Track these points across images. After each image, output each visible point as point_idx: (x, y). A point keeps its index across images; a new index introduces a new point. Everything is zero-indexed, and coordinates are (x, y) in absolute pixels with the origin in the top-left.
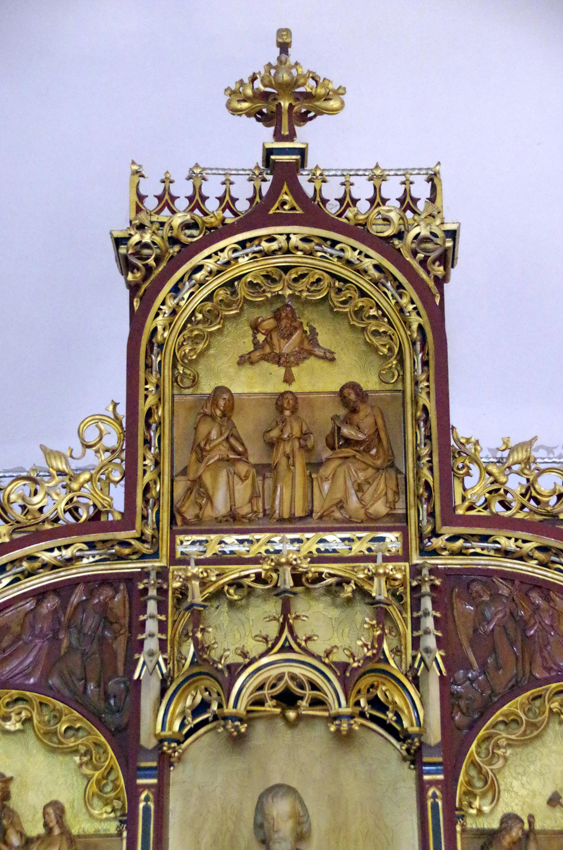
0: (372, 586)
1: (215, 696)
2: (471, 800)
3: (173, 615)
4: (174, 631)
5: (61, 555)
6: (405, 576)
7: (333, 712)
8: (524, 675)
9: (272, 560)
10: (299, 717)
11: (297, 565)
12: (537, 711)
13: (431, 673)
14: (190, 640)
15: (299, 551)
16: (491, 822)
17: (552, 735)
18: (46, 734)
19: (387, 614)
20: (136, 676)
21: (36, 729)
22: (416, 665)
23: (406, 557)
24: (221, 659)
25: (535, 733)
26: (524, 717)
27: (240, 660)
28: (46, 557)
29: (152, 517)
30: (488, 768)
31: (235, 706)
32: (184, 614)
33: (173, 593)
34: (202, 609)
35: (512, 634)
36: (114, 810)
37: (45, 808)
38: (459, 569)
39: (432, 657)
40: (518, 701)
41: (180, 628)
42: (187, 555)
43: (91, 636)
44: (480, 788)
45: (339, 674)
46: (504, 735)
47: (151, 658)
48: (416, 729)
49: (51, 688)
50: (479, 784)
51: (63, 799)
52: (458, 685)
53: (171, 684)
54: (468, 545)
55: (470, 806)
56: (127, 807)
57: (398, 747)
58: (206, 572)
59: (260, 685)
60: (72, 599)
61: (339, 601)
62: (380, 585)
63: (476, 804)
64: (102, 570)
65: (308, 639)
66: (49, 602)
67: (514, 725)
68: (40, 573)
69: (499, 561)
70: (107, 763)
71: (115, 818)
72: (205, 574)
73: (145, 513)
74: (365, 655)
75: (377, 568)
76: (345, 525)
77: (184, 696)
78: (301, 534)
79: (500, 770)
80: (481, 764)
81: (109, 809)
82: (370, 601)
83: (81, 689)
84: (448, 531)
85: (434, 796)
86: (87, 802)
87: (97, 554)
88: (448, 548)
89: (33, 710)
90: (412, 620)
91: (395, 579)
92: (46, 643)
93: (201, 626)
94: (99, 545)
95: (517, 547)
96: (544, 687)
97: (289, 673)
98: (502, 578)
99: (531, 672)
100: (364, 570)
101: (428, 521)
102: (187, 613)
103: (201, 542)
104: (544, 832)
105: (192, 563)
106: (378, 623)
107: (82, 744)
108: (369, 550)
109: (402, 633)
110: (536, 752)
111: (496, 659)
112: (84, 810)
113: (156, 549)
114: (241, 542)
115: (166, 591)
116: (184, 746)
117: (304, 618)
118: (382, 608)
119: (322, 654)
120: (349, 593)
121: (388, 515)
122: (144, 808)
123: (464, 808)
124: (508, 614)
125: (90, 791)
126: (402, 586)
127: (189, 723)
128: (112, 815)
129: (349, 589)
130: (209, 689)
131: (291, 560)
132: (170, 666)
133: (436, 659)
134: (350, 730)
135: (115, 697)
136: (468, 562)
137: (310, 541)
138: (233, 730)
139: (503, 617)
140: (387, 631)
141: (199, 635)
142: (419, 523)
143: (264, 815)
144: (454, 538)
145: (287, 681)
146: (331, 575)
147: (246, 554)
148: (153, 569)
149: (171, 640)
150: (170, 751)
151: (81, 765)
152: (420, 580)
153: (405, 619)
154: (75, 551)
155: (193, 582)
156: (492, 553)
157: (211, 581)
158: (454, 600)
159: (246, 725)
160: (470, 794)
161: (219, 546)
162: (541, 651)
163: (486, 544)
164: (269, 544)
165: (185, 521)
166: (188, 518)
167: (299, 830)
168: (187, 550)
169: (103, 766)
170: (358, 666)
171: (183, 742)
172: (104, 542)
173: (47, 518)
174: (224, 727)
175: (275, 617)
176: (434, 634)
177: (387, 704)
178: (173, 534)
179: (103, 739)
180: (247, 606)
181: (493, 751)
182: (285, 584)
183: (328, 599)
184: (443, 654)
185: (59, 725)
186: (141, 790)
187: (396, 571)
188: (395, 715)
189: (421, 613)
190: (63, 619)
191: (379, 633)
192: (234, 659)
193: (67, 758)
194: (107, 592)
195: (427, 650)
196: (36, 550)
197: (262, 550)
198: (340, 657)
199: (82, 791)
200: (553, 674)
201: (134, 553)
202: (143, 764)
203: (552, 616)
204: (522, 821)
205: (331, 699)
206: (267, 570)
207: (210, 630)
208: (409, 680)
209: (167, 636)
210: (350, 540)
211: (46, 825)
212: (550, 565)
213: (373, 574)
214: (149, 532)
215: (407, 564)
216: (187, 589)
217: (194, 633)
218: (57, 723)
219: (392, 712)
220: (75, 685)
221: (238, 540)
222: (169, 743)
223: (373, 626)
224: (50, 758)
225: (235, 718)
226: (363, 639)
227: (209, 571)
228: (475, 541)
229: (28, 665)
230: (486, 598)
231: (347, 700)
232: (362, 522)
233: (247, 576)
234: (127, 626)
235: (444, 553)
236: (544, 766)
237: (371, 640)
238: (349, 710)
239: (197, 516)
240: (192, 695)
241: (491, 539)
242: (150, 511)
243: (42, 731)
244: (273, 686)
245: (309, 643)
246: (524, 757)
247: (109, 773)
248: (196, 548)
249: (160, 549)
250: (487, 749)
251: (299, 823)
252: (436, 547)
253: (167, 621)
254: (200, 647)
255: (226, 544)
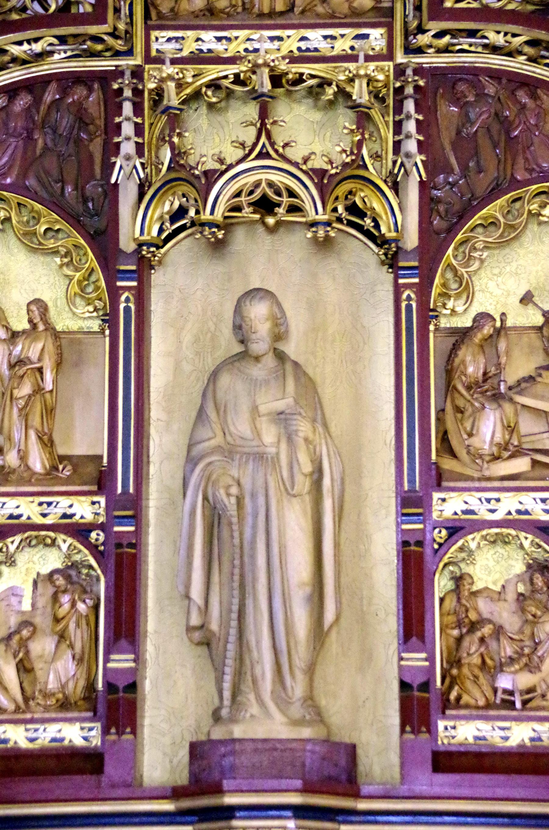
0: (353, 87)
1: (192, 202)
2: (446, 302)
3: (150, 118)
4: (151, 136)
5: (30, 49)
6: (388, 76)
7: (310, 219)
8: (505, 179)
9: (249, 62)
10: (279, 224)
11: (275, 66)
12: (516, 213)
13: (411, 178)
14: (167, 144)
15: (279, 50)
16: (465, 321)
17: (530, 236)
18: (25, 234)
19: (368, 117)
20: (113, 181)
21: (16, 230)
22: (396, 171)
23: (390, 56)
24: (198, 164)
25: (513, 235)
26: (502, 220)
27: (217, 166)
28: (15, 50)
29: (125, 10)
30: (463, 270)
31: (212, 213)
32: (161, 117)
33: (150, 94)
34: (178, 112)
35: (496, 137)
36: (96, 310)
37: (29, 304)
38: (446, 67)
39: (412, 162)
40: (497, 204)
41: (157, 132)
42: (163, 53)
43: (66, 136)
44: (456, 290)
45: (316, 181)
46: (482, 238)
47: (128, 162)
48: (393, 234)
49: (27, 188)
50: (454, 286)
51: (45, 298)
52: (439, 190)
53: (148, 190)
54: (455, 41)
55: (444, 306)
56: (108, 307)
57: (377, 251)
58: (182, 73)
59: (238, 192)
60: (44, 98)
61: (320, 103)
62: (361, 86)
63: (450, 305)
64: (76, 67)
65: (286, 145)
66: (22, 99)
67: (492, 228)
68: (11, 68)
69: (488, 58)
70: (87, 265)
71: (98, 317)
72: (181, 75)
73: (117, 5)
74: (344, 161)
75: (358, 68)
76: (327, 21)
77: (162, 202)
78: (281, 31)
79: (475, 272)
80: (457, 267)
81: (91, 308)
82: (350, 104)
83: (59, 191)
84: (435, 26)
85: (409, 298)
86: (70, 301)
87: (69, 50)
88: (434, 45)
89: (11, 209)
90: (394, 124)
91: (377, 81)
92: (20, 143)
93: (178, 131)
94: (70, 40)
95: (506, 42)
96: (524, 189)
97: (266, 179)
98: (489, 77)
99: (512, 175)
100: (345, 71)
101: (414, 16)
102: (163, 116)
103: (177, 39)
104: (515, 328)
105: (168, 62)
106: (358, 128)
107: (62, 246)
108: (352, 48)
109: (383, 138)
110: (513, 253)
111: (478, 163)
112: (67, 309)
113: (130, 45)
114: (219, 39)
115: (142, 92)
116: (163, 251)
117: (282, 124)
118: (362, 112)
119: (300, 161)
120: (330, 95)
121: (373, 8)
122: (125, 308)
123: (438, 310)
124: (493, 114)
125: (71, 292)
126: (385, 87)
127: (168, 229)
128: (95, 314)
129: (330, 91)
130: (187, 196)
131: (269, 61)
132: (148, 170)
133: (416, 164)
134: (327, 238)
135: (93, 200)
136: (455, 60)
137: (291, 39)
138: (210, 236)
139: (487, 119)
140: (367, 136)
141: (176, 140)
142: (404, 19)
143: (242, 318)
144: (439, 35)
145: (264, 188)
146: (313, 77)
147: (224, 53)
148: (127, 68)
149: (148, 143)
150: (149, 255)
151: (61, 266)
152: (403, 81)
153: (387, 123)
154: (45, 45)
155: (169, 83)
156: (480, 49)
157: (187, 83)
158: (438, 102)
159: (223, 232)
160: (445, 295)
161: (196, 43)
162: (524, 152)
163: (473, 40)
164: (248, 42)
165: (160, 16)
166: (164, 12)
167: (277, 331)
168: (162, 47)
169: (83, 268)
170: (336, 173)
171: (162, 247)
172: (75, 36)
173: (14, 7)
174: (201, 233)
175: (252, 122)
176: (415, 138)
177: (365, 211)
178: (148, 29)
179: (82, 242)
180: (226, 109)
181: (469, 253)
182: (263, 87)
183: (310, 101)
184: (424, 158)
185: (38, 227)
186: (121, 292)
187: (378, 72)
188: (373, 221)
189: (402, 137)
190: (36, 118)
191: (359, 137)
192: (212, 165)
193: (48, 259)
194: (80, 92)
195: (408, 155)
196: (4, 43)
197: (241, 49)
198: (318, 163)
199: (64, 290)
200: (534, 175)
201: (107, 50)
202: (122, 268)
203: (538, 115)
204: (494, 320)
205: (308, 206)
206: (245, 72)
207: (187, 134)
208: (388, 186)
209: (144, 139)
210: (333, 38)
211: (30, 321)
212: (539, 60)
213: (354, 75)
214: (122, 26)
215: (391, 64)
216: (163, 90)
217: (171, 137)
218: (37, 224)
219: (370, 218)
220: (52, 187)
221: (216, 38)
222: (148, 248)
223: (352, 131)
224: (32, 258)
225: (212, 224)
226: (341, 144)
227: (185, 72)
228: (463, 37)
229: (5, 164)
230: (471, 98)
231: (324, 207)
232: (346, 17)
233: (226, 77)
234: (103, 127)
235: (429, 51)
236: (520, 267)
237: (350, 146)
238: (326, 217)
239: (172, 10)
240: (170, 200)
241: (479, 34)
242: (122, 3)
243: (21, 232)
244: (251, 193)
245: (287, 149)
246: (501, 259)
247: (90, 275)
248: (173, 46)
249: (134, 45)
250: (464, 252)
251: (277, 325)
252: (421, 44)
253: (143, 124)
254: (176, 152)
255: (203, 41)
